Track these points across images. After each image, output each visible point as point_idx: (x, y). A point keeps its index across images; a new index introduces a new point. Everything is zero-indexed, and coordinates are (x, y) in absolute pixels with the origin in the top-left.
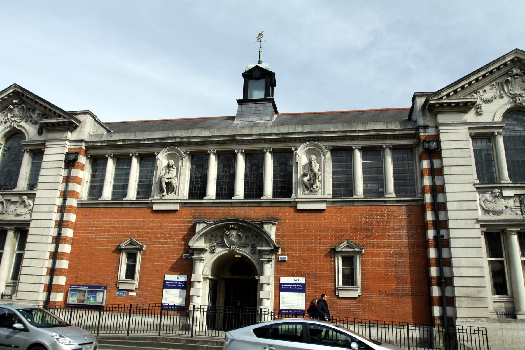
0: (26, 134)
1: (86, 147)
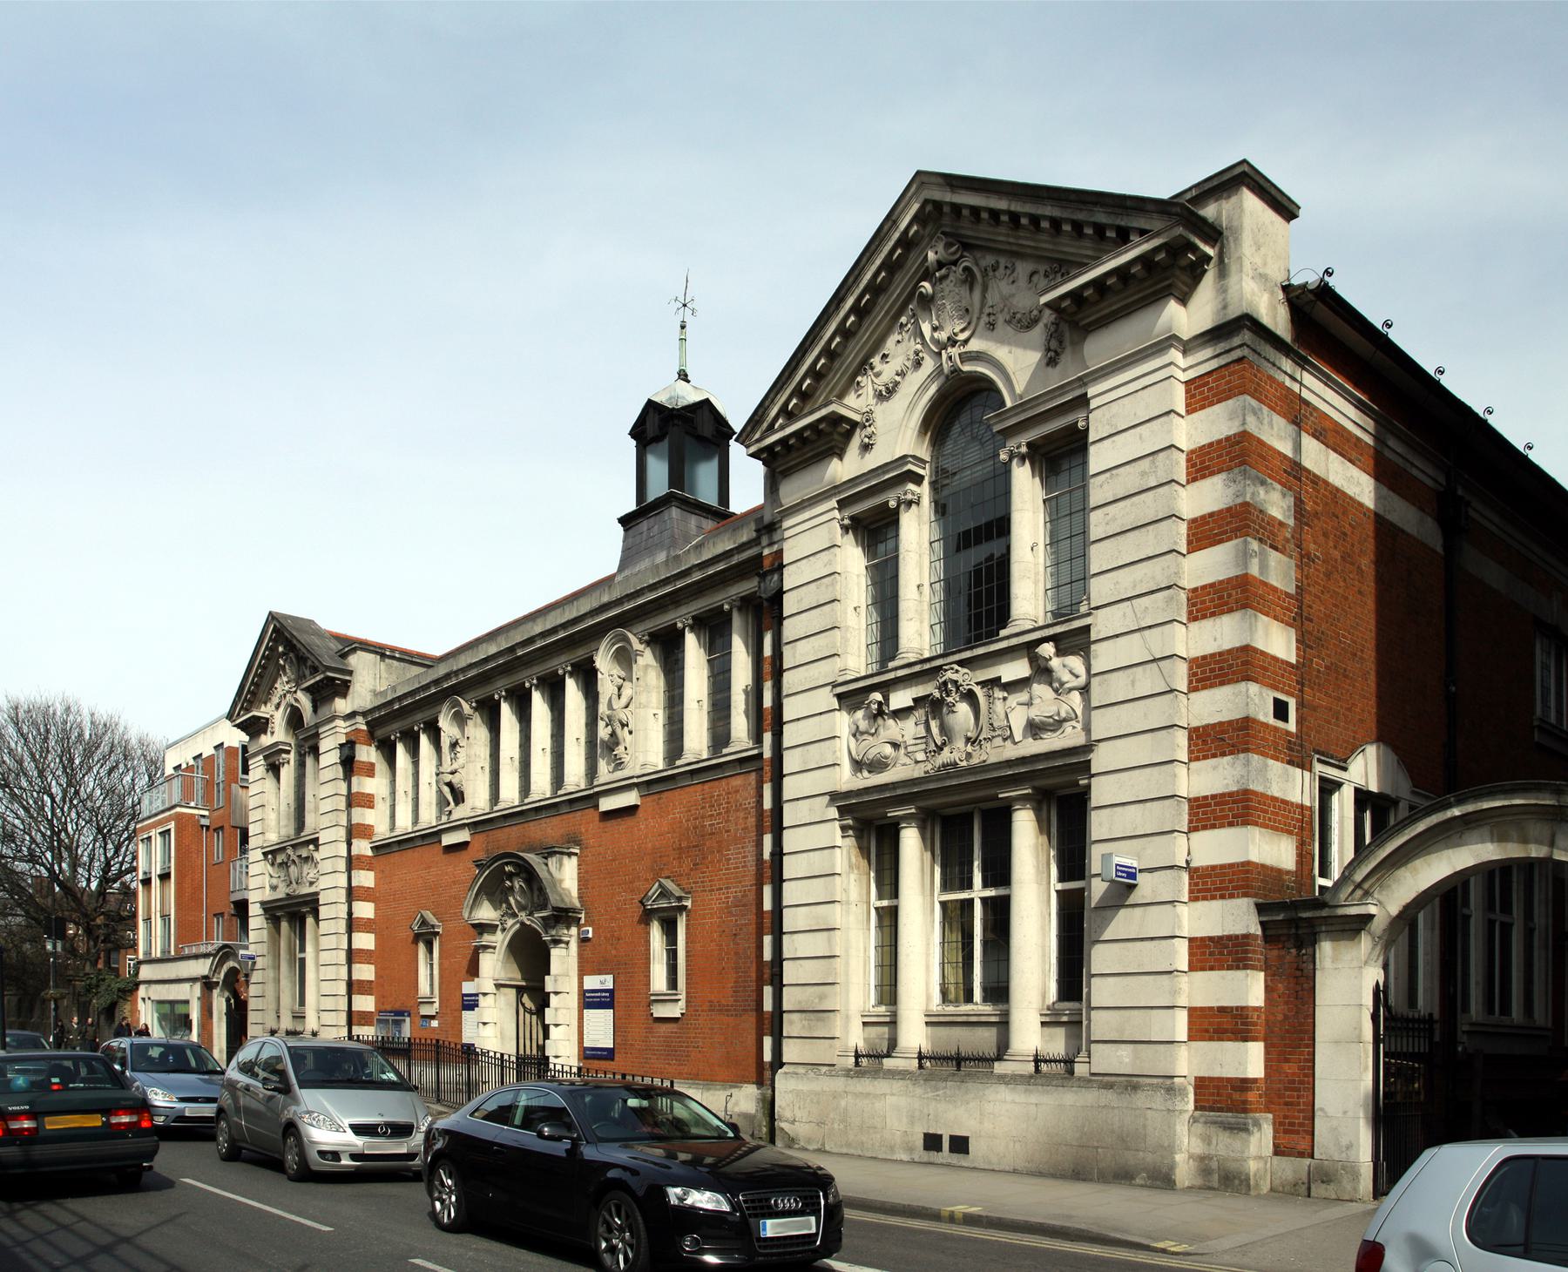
0: (1000, 385)
1: (367, 723)
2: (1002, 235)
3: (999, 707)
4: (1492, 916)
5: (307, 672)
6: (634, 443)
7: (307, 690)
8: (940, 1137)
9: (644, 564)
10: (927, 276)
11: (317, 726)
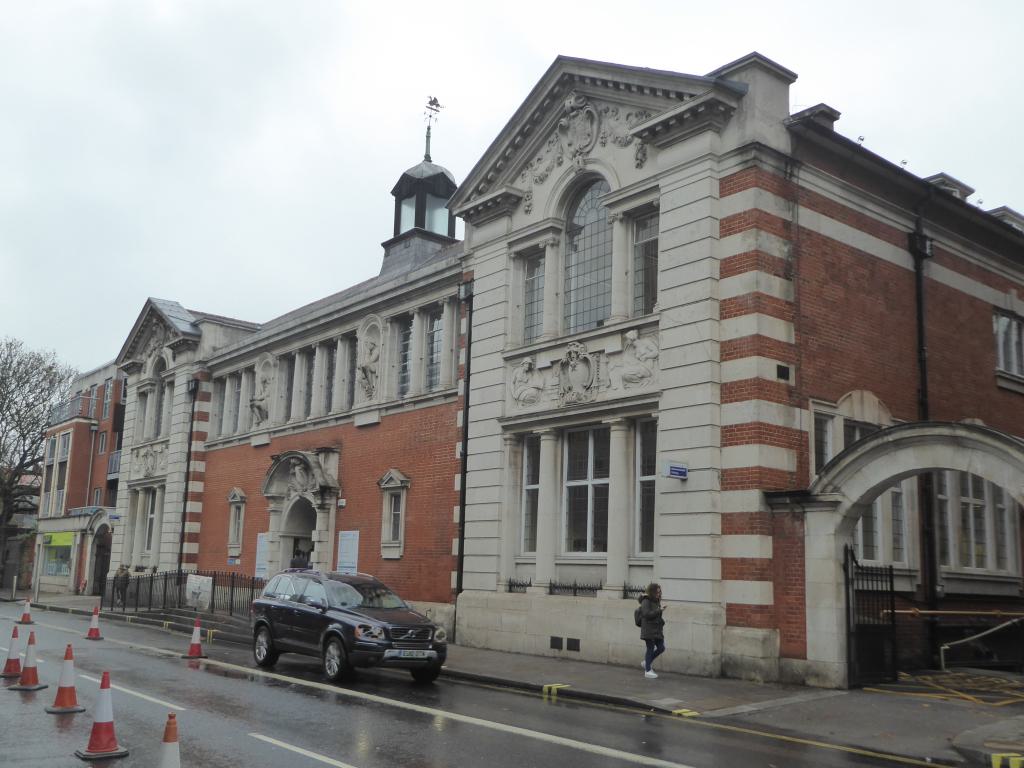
2: (610, 93)
3: (602, 366)
4: (964, 499)
5: (171, 336)
6: (394, 198)
7: (169, 346)
8: (561, 639)
9: (397, 272)
10: (565, 115)
11: (174, 369)
